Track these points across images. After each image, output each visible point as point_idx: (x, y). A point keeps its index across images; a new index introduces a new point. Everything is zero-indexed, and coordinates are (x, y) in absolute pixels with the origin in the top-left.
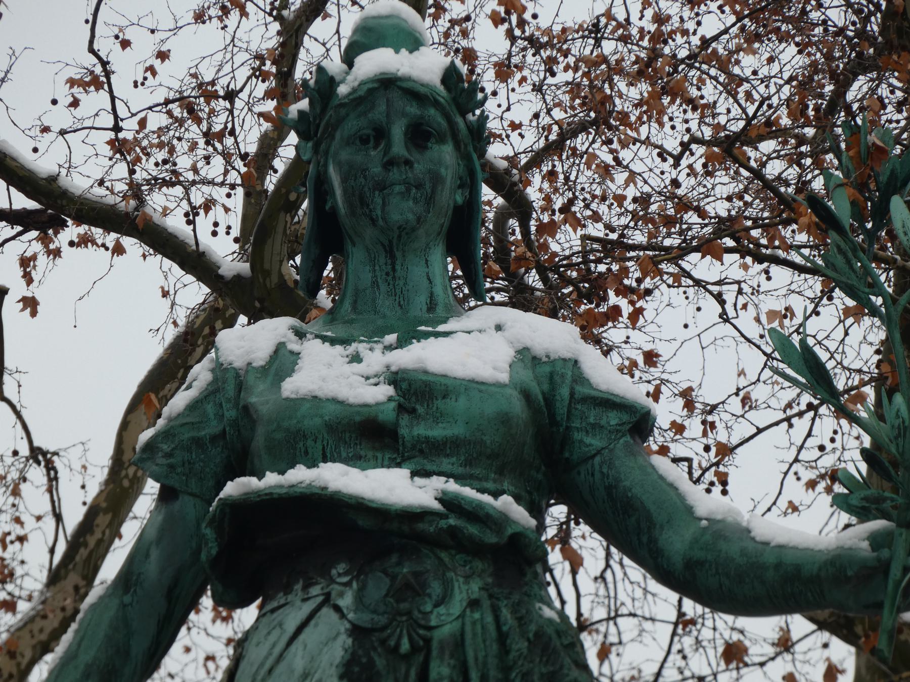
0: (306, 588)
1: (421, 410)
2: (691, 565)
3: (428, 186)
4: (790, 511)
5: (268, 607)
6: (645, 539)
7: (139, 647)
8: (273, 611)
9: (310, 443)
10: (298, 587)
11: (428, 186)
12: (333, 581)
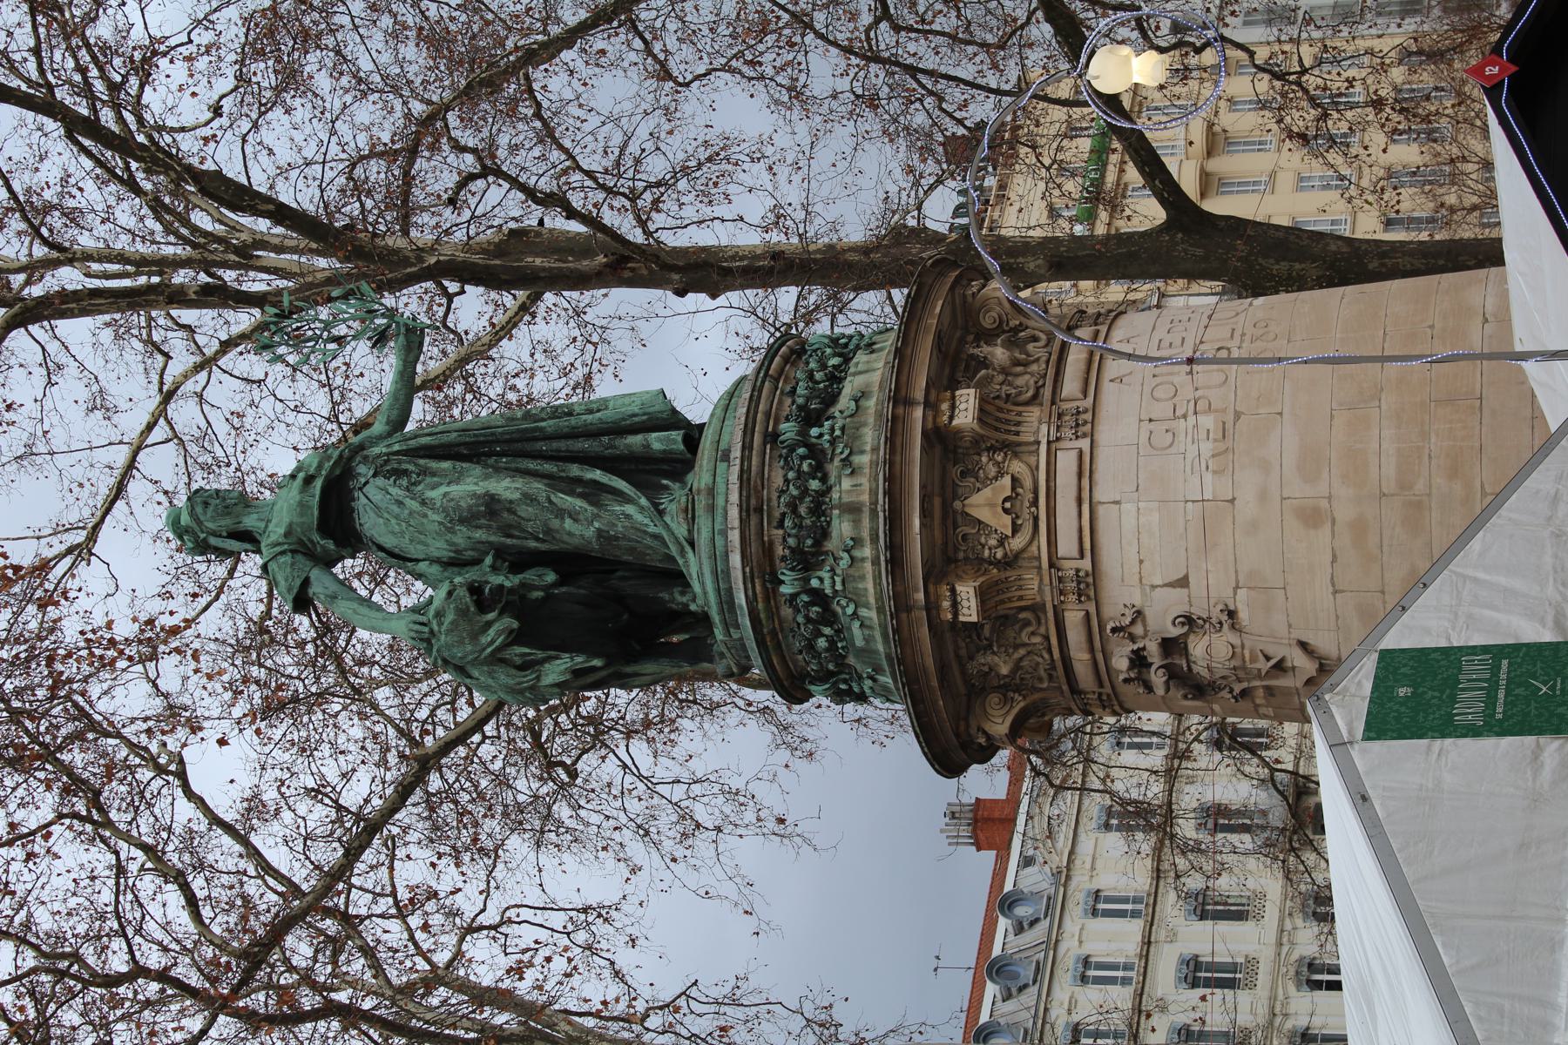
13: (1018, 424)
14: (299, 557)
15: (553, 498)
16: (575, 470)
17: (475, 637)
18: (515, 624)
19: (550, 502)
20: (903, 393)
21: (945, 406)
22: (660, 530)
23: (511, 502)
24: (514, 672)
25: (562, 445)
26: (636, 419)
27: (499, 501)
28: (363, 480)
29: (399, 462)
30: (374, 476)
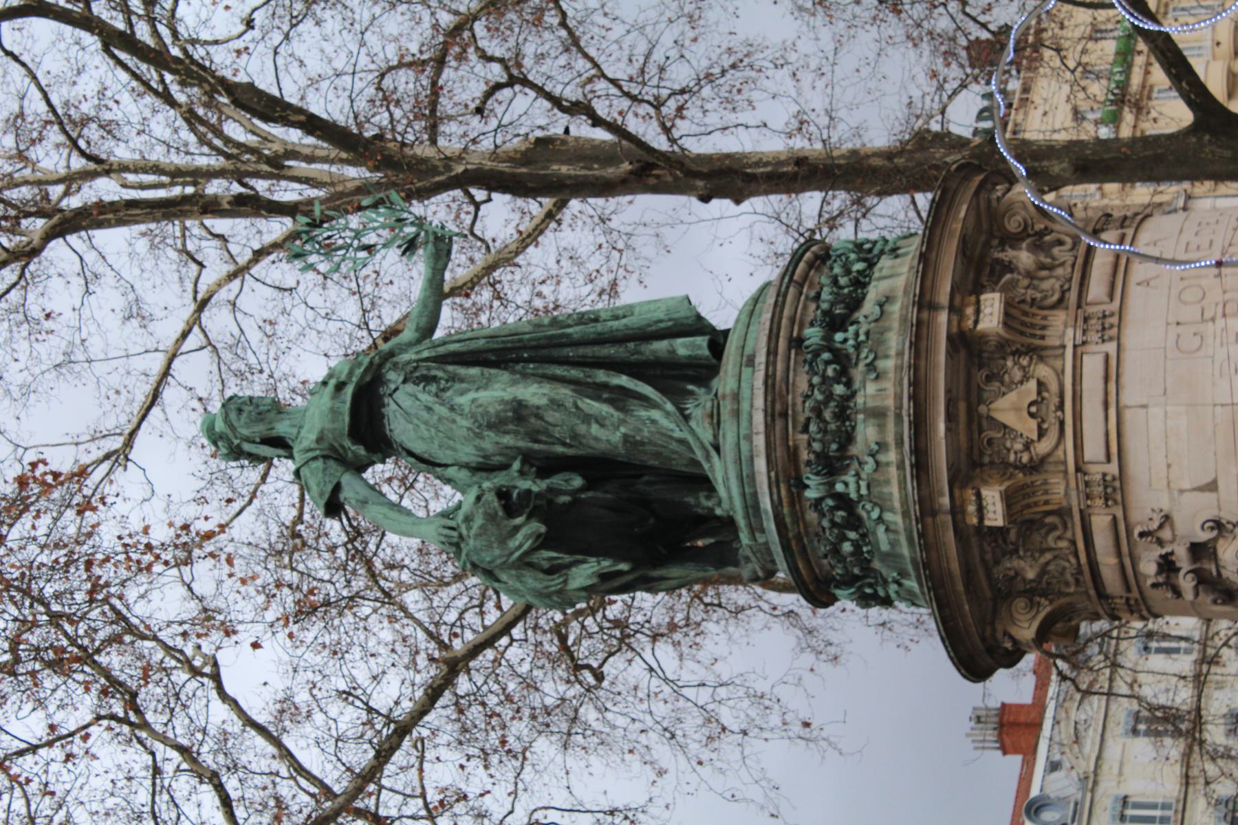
13: (1044, 328)
14: (331, 463)
15: (580, 403)
16: (601, 376)
17: (503, 541)
18: (543, 529)
19: (577, 407)
20: (927, 297)
21: (970, 311)
22: (685, 435)
23: (538, 408)
24: (541, 575)
25: (588, 351)
26: (662, 325)
27: (526, 406)
28: (393, 387)
29: (429, 369)
30: (404, 382)
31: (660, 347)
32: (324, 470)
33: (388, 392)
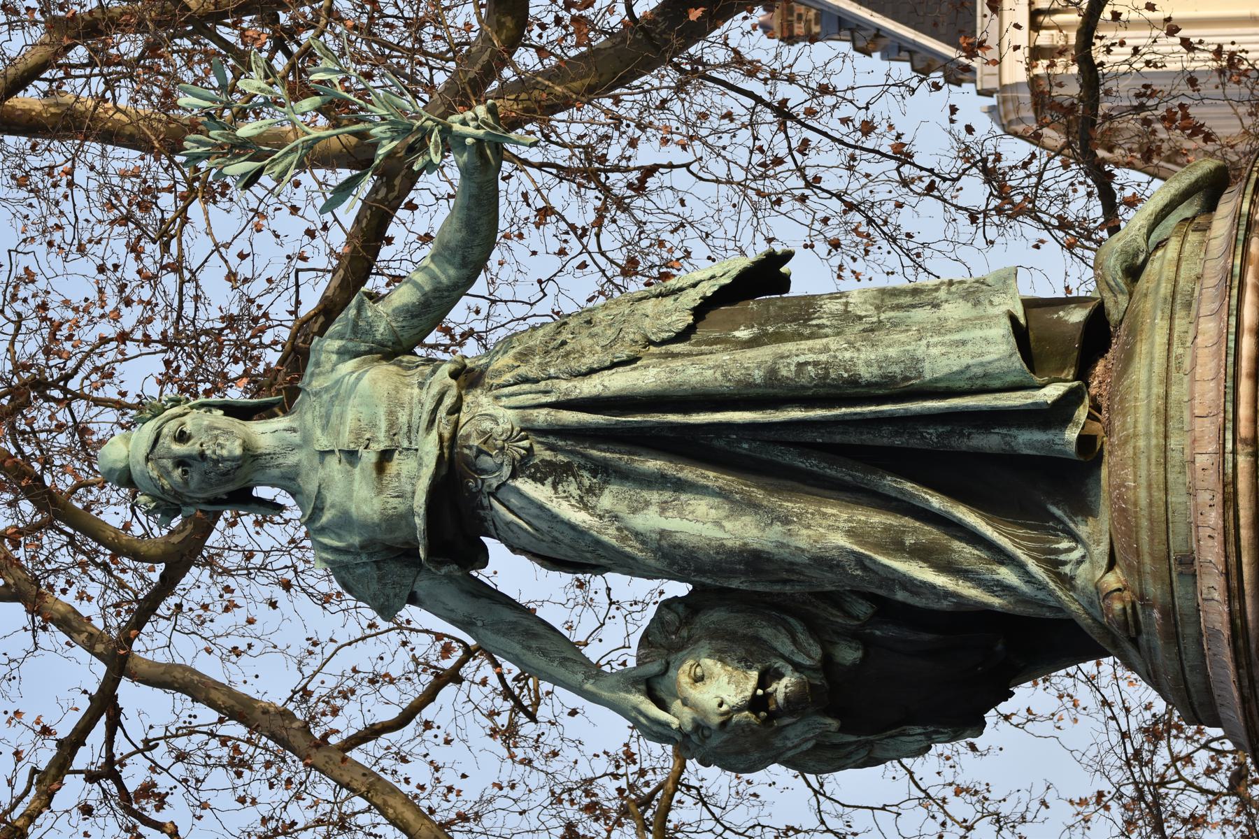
0: (483, 508)
1: (368, 436)
2: (464, 264)
3: (216, 432)
4: (936, 193)
5: (493, 532)
6: (446, 294)
7: (509, 615)
8: (496, 529)
9: (388, 506)
10: (482, 513)
11: (216, 432)
12: (480, 491)
15: (867, 562)
19: (864, 568)
23: (791, 563)
31: (990, 441)
32: (380, 579)
33: (486, 489)
